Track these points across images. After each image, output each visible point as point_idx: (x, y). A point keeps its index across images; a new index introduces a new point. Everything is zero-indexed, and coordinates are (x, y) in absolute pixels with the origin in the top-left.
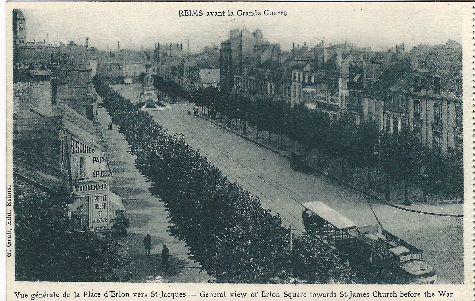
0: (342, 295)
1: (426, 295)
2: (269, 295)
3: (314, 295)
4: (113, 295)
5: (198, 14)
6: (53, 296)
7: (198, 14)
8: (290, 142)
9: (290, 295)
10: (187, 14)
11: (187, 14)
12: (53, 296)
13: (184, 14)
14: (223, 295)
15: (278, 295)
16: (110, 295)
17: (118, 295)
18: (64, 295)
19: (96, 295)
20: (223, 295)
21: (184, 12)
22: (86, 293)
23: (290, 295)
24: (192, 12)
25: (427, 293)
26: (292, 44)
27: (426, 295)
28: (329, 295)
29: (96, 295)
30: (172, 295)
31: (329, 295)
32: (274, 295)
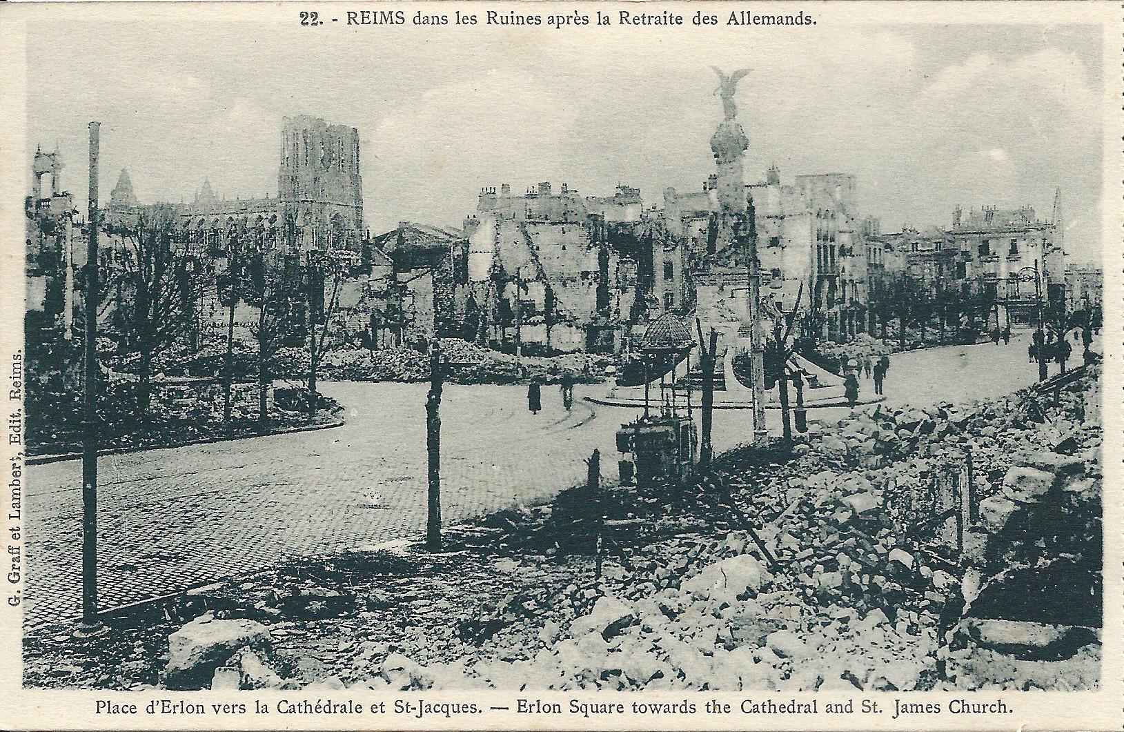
0: (399, 709)
2: (535, 709)
3: (643, 709)
4: (523, 709)
6: (348, 710)
8: (860, 574)
11: (366, 20)
12: (348, 710)
13: (359, 19)
14: (812, 709)
15: (679, 20)
16: (158, 709)
17: (178, 710)
19: (438, 709)
20: (812, 709)
22: (101, 704)
24: (379, 15)
26: (705, 119)
27: (711, 709)
28: (677, 709)
30: (445, 708)
31: (677, 709)
32: (547, 709)
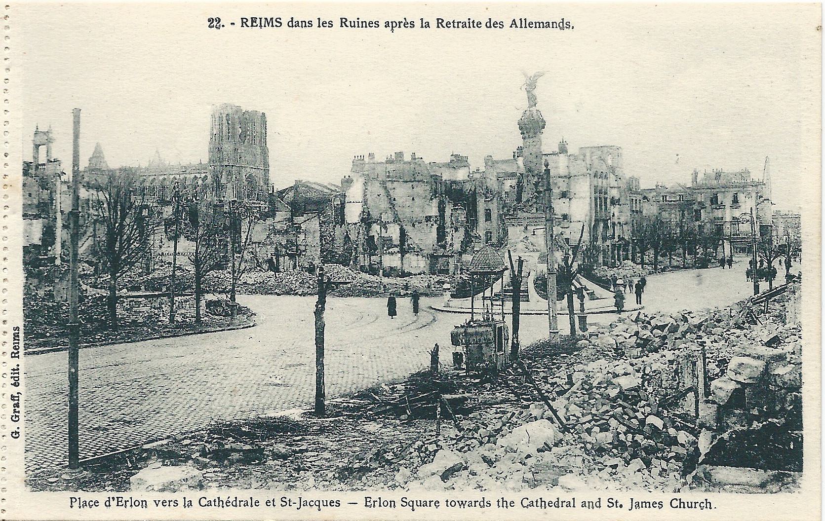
1: (501, 504)
2: (377, 504)
3: (453, 504)
5: (275, 23)
6: (249, 504)
7: (275, 23)
9: (411, 504)
10: (254, 24)
11: (254, 24)
12: (249, 504)
13: (249, 23)
14: (572, 505)
18: (290, 24)
19: (91, 503)
20: (572, 505)
21: (250, 21)
22: (74, 500)
23: (411, 504)
24: (263, 21)
25: (501, 500)
27: (501, 504)
29: (91, 503)
31: (477, 504)
